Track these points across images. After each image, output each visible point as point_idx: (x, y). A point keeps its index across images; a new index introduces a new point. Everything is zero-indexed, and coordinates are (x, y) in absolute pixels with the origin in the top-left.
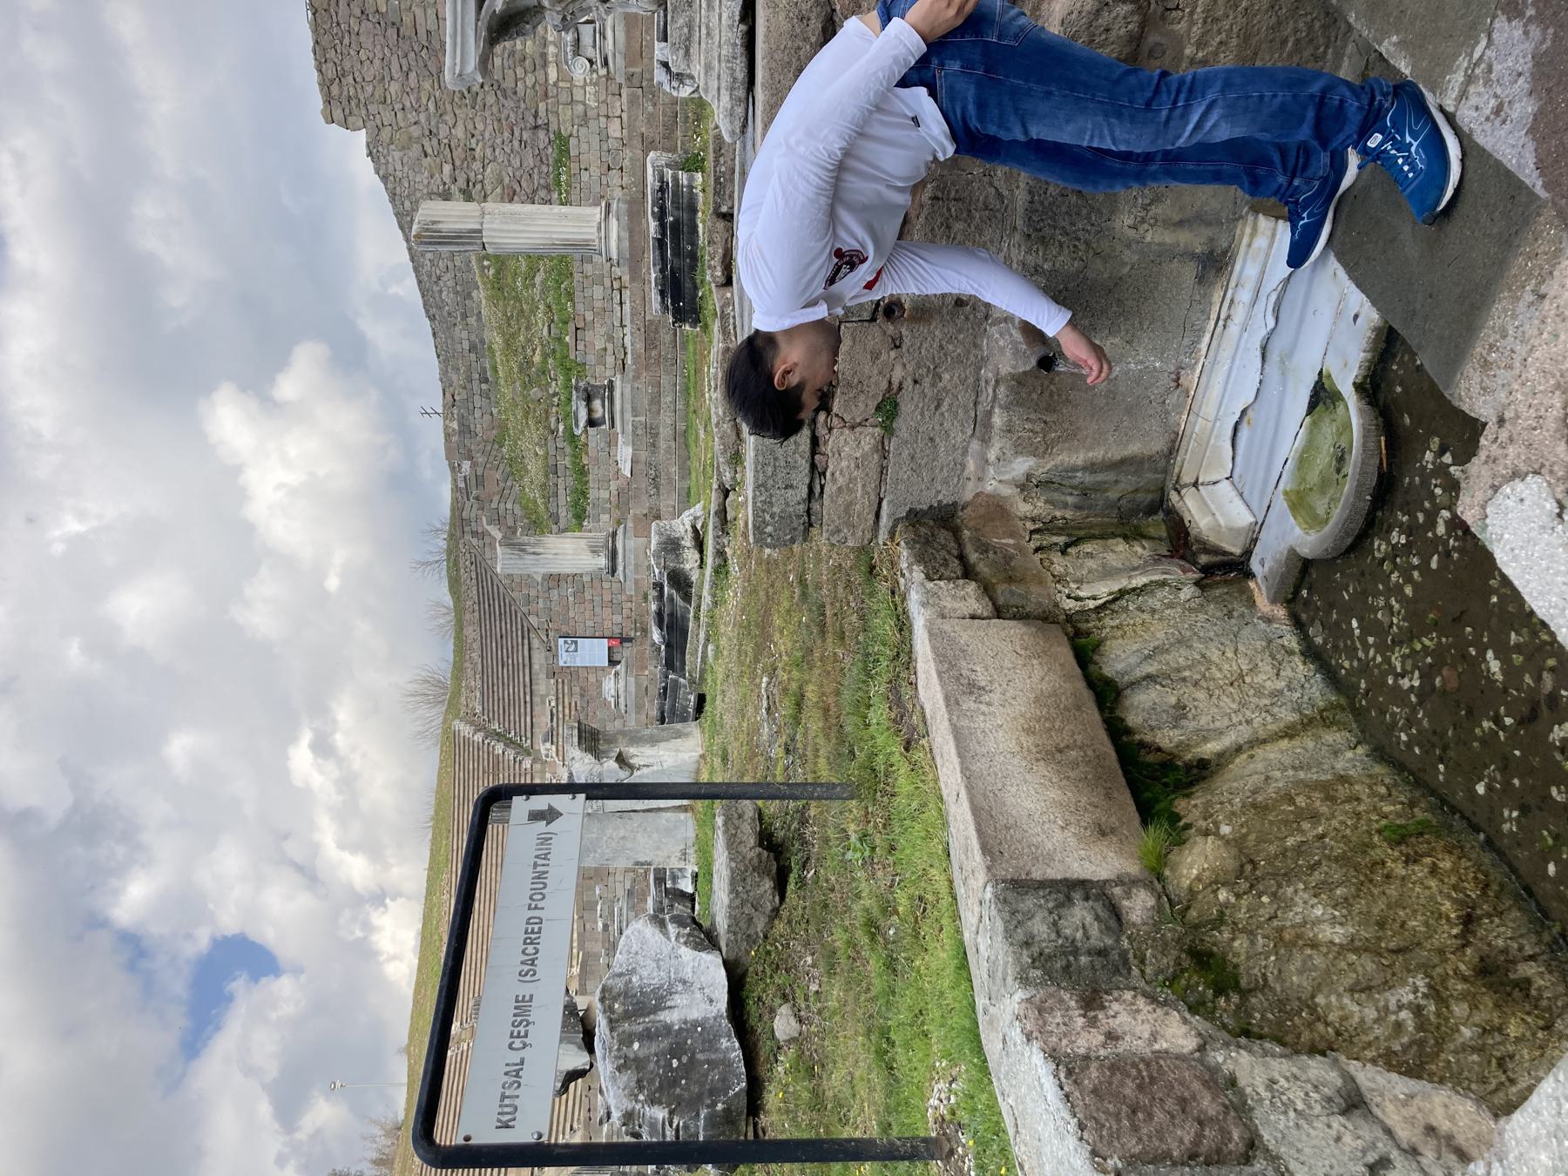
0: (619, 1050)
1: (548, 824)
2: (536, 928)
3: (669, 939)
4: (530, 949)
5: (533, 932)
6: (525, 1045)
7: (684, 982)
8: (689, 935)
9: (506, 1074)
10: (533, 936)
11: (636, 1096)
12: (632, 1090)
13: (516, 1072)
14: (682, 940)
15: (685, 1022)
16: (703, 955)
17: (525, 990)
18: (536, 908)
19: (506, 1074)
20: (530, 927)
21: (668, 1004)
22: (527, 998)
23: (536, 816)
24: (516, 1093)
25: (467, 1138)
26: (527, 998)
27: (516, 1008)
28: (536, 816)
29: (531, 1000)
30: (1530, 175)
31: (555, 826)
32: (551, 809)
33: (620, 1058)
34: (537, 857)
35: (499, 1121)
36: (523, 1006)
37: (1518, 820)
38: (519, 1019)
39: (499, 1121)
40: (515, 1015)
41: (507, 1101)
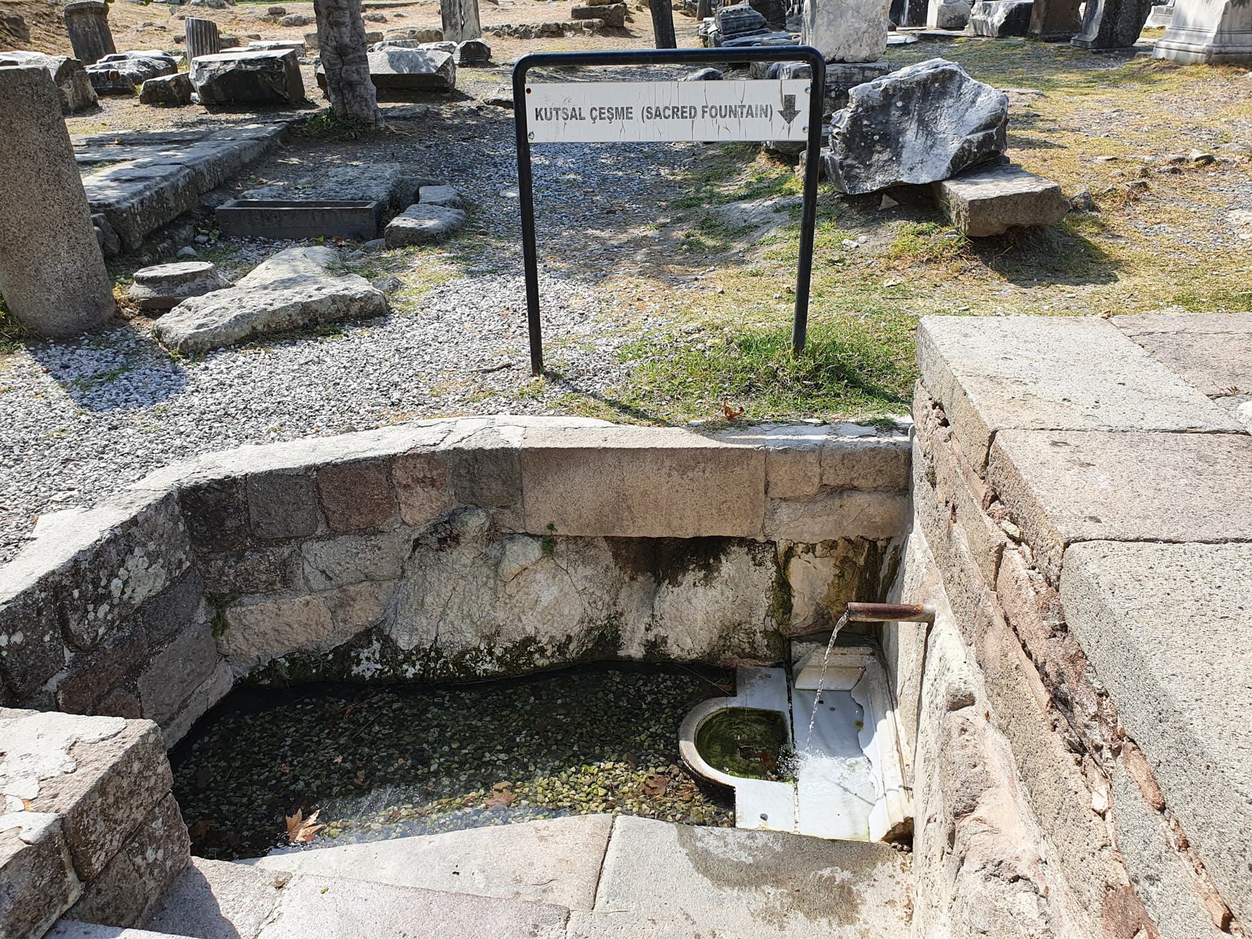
0: (901, 89)
1: (781, 112)
2: (688, 114)
3: (970, 134)
4: (668, 112)
5: (683, 112)
6: (594, 119)
7: (931, 147)
8: (970, 151)
9: (574, 109)
10: (679, 113)
11: (862, 106)
12: (867, 102)
13: (575, 115)
14: (965, 145)
15: (902, 147)
16: (947, 163)
17: (636, 113)
18: (704, 112)
19: (574, 109)
20: (688, 110)
21: (921, 132)
22: (630, 115)
23: (789, 102)
24: (560, 118)
25: (529, 91)
26: (630, 115)
27: (622, 108)
28: (789, 102)
29: (628, 118)
30: (197, 861)
31: (778, 118)
32: (796, 113)
33: (894, 91)
34: (750, 107)
35: (541, 109)
36: (623, 113)
37: (493, 719)
38: (614, 112)
39: (541, 109)
40: (617, 108)
41: (554, 112)
